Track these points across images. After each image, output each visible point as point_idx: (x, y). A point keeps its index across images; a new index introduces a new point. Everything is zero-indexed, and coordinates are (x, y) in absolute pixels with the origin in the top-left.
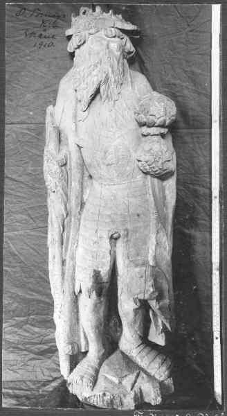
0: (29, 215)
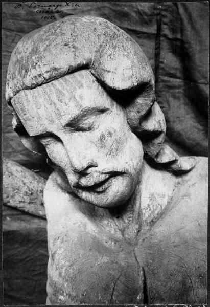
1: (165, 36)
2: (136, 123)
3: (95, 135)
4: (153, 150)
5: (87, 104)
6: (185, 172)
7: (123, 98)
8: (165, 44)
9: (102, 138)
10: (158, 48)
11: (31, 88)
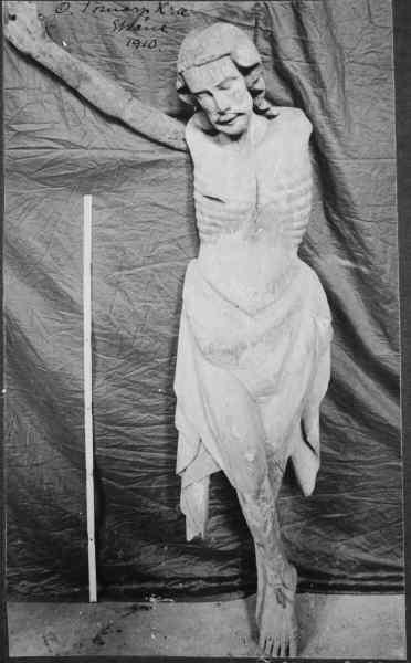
0: (178, 245)
1: (261, 28)
2: (250, 85)
3: (230, 92)
4: (257, 102)
5: (228, 75)
6: (274, 117)
7: (245, 71)
8: (260, 33)
9: (234, 94)
10: (255, 36)
11: (199, 66)
